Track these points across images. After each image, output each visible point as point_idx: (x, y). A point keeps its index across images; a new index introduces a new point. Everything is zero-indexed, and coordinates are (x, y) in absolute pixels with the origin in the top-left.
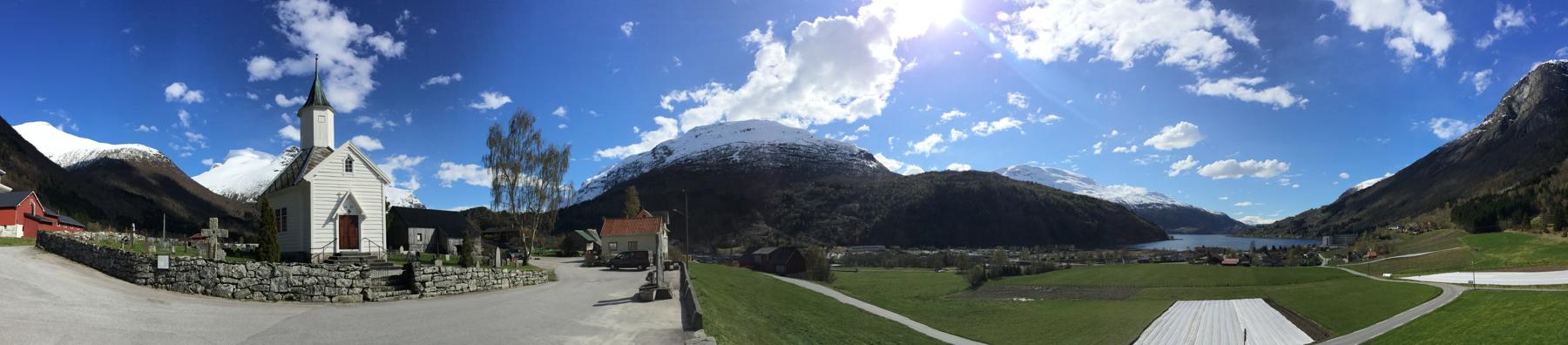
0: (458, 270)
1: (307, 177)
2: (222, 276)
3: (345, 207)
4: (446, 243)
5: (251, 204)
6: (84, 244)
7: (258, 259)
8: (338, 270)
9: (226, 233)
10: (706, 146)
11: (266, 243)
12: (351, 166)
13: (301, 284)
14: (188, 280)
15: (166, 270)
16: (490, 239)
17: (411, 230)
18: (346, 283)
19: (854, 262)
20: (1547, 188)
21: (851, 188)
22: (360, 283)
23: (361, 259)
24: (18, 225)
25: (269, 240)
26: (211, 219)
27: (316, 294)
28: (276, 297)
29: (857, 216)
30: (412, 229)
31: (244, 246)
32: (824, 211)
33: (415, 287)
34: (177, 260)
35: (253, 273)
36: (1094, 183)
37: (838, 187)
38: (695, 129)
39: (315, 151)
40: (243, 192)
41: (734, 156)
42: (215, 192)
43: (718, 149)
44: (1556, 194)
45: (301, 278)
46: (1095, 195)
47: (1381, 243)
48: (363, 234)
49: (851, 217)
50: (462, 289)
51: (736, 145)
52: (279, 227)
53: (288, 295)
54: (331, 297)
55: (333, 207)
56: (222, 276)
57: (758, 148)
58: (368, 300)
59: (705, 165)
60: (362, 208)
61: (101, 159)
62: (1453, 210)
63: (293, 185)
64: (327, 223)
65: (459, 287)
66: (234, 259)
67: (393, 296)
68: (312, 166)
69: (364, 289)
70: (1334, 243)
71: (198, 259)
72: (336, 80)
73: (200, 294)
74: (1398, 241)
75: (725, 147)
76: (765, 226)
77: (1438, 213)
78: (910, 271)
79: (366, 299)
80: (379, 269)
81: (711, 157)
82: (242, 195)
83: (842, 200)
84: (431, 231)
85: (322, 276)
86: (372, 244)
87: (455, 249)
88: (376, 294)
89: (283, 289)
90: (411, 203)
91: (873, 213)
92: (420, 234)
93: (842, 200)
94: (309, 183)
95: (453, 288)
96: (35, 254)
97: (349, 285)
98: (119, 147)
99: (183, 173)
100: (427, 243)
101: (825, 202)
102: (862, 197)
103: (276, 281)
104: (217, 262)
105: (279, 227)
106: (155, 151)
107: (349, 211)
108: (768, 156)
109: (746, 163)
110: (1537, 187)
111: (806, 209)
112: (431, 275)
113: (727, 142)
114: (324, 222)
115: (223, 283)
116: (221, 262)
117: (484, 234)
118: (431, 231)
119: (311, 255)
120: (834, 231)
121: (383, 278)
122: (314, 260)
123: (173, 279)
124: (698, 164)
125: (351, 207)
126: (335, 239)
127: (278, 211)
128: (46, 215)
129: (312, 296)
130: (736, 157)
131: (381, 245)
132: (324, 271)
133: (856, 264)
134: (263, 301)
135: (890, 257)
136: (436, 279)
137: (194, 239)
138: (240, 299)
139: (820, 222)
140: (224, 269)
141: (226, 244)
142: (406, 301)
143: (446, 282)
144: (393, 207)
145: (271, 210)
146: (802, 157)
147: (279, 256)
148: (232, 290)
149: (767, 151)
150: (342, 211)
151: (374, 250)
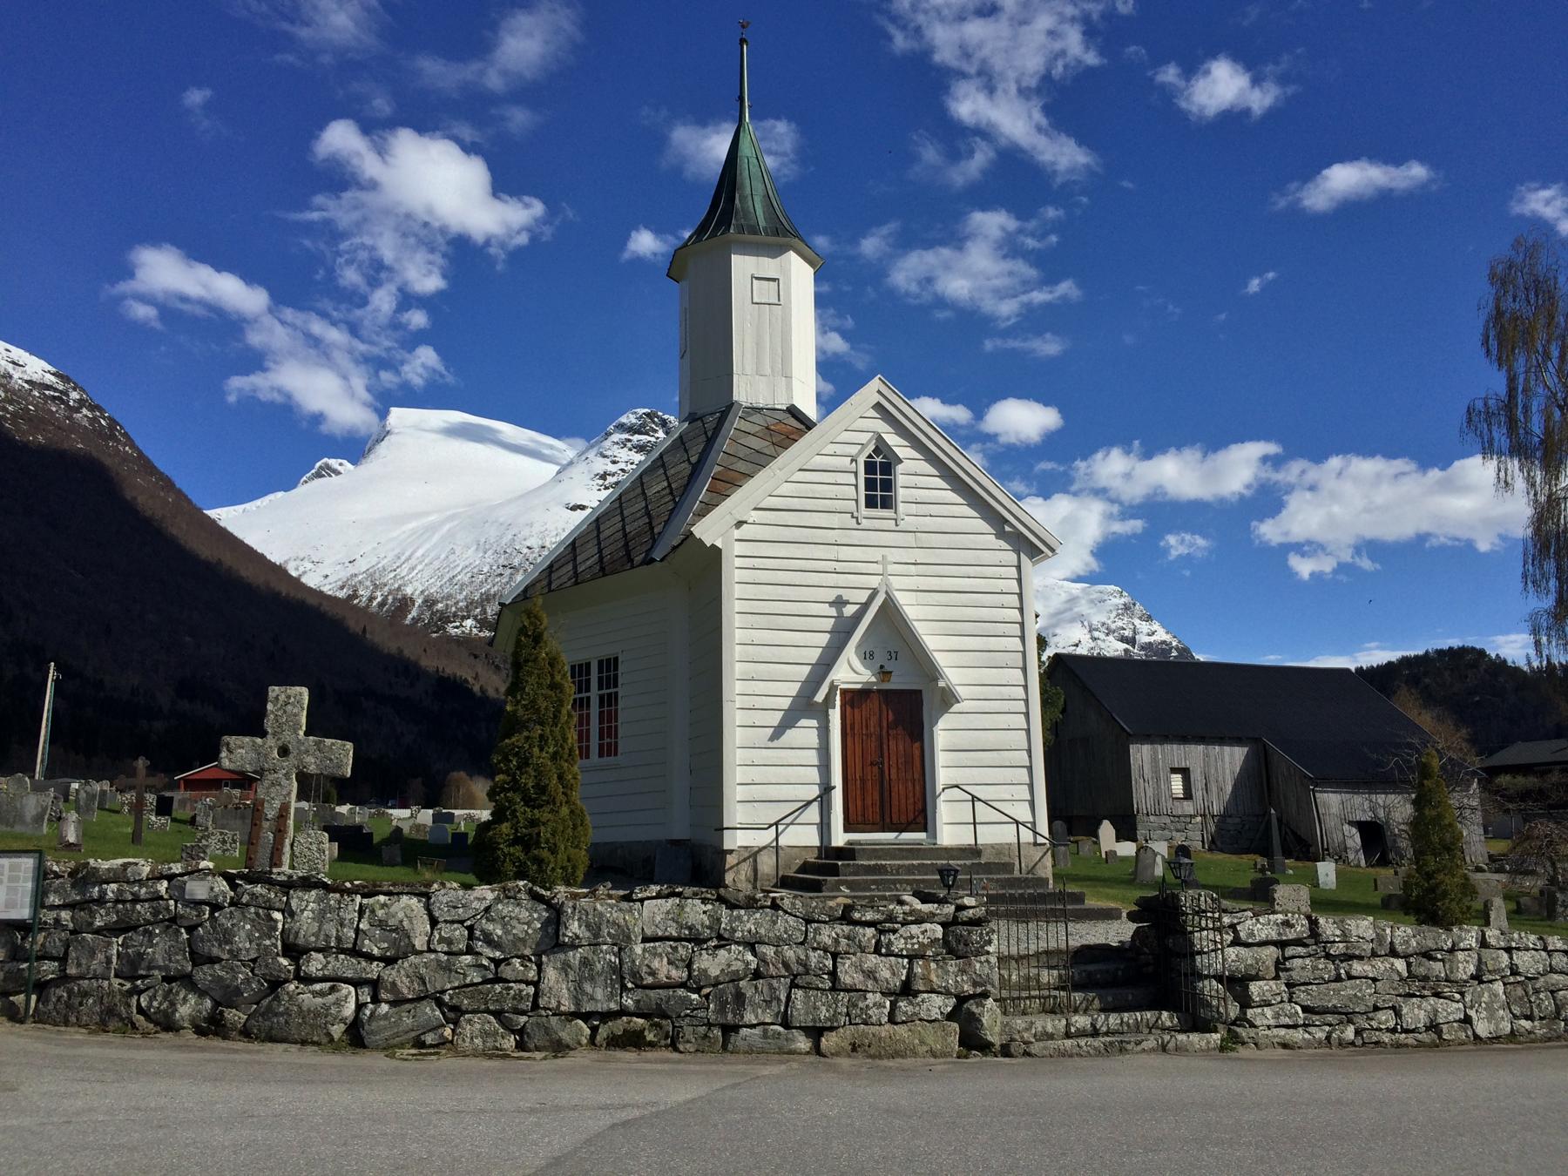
0: (1404, 933)
1: (709, 530)
3: (867, 656)
4: (1307, 808)
5: (465, 641)
7: (489, 874)
8: (846, 917)
9: (342, 756)
11: (527, 801)
12: (888, 485)
13: (678, 974)
14: (132, 968)
16: (1525, 795)
17: (1141, 755)
18: (885, 974)
22: (951, 975)
23: (944, 872)
25: (542, 789)
26: (274, 691)
27: (750, 1017)
28: (565, 1035)
30: (1146, 748)
31: (426, 816)
33: (1200, 1001)
34: (83, 878)
35: (460, 933)
39: (736, 423)
45: (683, 950)
48: (945, 771)
50: (1433, 1027)
52: (583, 736)
53: (618, 1026)
54: (815, 1033)
55: (814, 655)
56: (306, 951)
58: (985, 1047)
60: (941, 660)
63: (649, 561)
64: (789, 721)
65: (1416, 1013)
66: (371, 872)
67: (1095, 1033)
68: (727, 484)
69: (962, 999)
71: (194, 872)
72: (946, 12)
73: (189, 1035)
79: (973, 1041)
80: (1022, 917)
82: (429, 602)
84: (1232, 758)
85: (778, 943)
86: (983, 812)
87: (1354, 839)
88: (1019, 1023)
89: (600, 997)
90: (1131, 641)
92: (1185, 772)
94: (716, 553)
95: (1386, 1018)
97: (896, 983)
99: (169, 484)
100: (1217, 808)
104: (288, 886)
105: (583, 736)
107: (884, 673)
112: (1271, 952)
114: (775, 718)
115: (308, 980)
116: (307, 884)
117: (1494, 771)
118: (1232, 758)
119: (723, 853)
121: (1048, 957)
122: (737, 878)
125: (893, 655)
126: (827, 789)
127: (581, 670)
129: (729, 1030)
131: (1023, 813)
132: (787, 924)
134: (501, 1055)
136: (1301, 966)
137: (191, 784)
138: (389, 1048)
140: (320, 917)
141: (344, 809)
142: (1158, 1060)
143: (1348, 989)
144: (1057, 656)
145: (553, 661)
147: (582, 858)
148: (349, 1009)
150: (851, 672)
151: (995, 835)
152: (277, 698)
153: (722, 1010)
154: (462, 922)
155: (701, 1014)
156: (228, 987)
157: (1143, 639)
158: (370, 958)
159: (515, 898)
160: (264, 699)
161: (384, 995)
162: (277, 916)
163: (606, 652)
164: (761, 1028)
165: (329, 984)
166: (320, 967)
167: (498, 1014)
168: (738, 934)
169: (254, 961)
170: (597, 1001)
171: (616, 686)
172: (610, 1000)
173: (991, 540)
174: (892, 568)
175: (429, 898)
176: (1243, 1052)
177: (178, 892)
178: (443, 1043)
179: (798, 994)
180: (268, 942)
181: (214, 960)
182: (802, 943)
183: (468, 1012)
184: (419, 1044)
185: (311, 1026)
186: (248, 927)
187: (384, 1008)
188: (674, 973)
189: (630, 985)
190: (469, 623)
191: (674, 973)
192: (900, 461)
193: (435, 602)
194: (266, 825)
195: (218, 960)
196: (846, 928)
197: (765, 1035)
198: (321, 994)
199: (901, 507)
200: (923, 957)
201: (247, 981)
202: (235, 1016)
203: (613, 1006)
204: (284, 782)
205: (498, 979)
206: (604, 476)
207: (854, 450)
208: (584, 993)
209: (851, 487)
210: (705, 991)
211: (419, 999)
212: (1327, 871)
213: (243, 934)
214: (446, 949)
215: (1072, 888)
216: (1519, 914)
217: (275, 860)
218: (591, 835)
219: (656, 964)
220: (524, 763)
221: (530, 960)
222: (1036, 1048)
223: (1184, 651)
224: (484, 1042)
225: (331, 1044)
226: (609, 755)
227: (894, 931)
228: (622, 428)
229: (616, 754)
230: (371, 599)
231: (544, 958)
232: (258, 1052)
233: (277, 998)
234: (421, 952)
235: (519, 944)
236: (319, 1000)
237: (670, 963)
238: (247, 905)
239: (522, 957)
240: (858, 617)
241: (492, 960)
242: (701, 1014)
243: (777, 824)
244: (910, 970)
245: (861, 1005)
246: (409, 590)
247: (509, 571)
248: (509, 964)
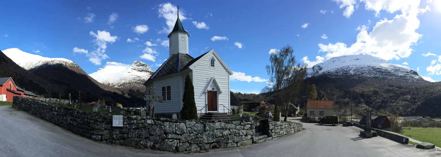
2: (168, 133)
3: (211, 86)
5: (116, 88)
6: (46, 105)
10: (337, 66)
12: (213, 64)
13: (221, 135)
15: (120, 128)
19: (408, 125)
21: (406, 88)
24: (4, 95)
27: (230, 142)
29: (409, 102)
32: (393, 99)
37: (400, 88)
38: (333, 58)
40: (113, 82)
41: (351, 71)
42: (99, 82)
43: (343, 68)
49: (406, 102)
51: (352, 66)
53: (213, 145)
54: (237, 143)
55: (204, 86)
56: (168, 133)
57: (362, 68)
59: (337, 75)
60: (220, 87)
61: (44, 64)
71: (147, 118)
75: (347, 67)
76: (365, 105)
78: (436, 129)
81: (340, 72)
82: (112, 84)
83: (403, 94)
91: (417, 100)
93: (403, 94)
94: (192, 70)
96: (12, 111)
98: (53, 59)
101: (394, 94)
102: (412, 92)
103: (206, 134)
106: (71, 62)
107: (213, 89)
108: (367, 72)
109: (356, 75)
111: (384, 98)
113: (348, 65)
114: (199, 94)
115: (169, 139)
120: (398, 109)
123: (125, 135)
124: (334, 75)
128: (18, 90)
130: (352, 72)
133: (409, 125)
135: (425, 122)
138: (182, 152)
139: (391, 104)
146: (383, 73)
149: (366, 69)
150: (209, 89)
152: (152, 89)
153: (226, 141)
154: (191, 127)
155: (224, 141)
156: (156, 140)
158: (178, 134)
159: (198, 123)
161: (181, 141)
162: (163, 127)
164: (231, 143)
165: (172, 140)
166: (170, 136)
167: (197, 144)
168: (228, 128)
169: (160, 135)
170: (211, 141)
171: (170, 90)
172: (212, 140)
173: (225, 72)
174: (215, 75)
175: (185, 123)
179: (235, 137)
180: (162, 132)
182: (235, 129)
183: (193, 144)
185: (170, 148)
186: (158, 129)
187: (181, 144)
188: (220, 135)
189: (215, 137)
190: (117, 86)
191: (220, 135)
192: (215, 61)
193: (113, 84)
194: (151, 110)
195: (153, 135)
196: (240, 126)
197: (231, 144)
198: (171, 142)
199: (215, 67)
200: (248, 130)
201: (159, 139)
202: (157, 146)
203: (213, 141)
204: (153, 103)
205: (197, 138)
206: (132, 69)
207: (210, 58)
208: (209, 139)
209: (209, 63)
210: (224, 137)
211: (186, 142)
213: (157, 130)
214: (189, 132)
219: (218, 133)
221: (201, 134)
224: (195, 149)
226: (169, 100)
227: (245, 126)
228: (134, 63)
229: (170, 100)
230: (106, 84)
231: (203, 134)
232: (164, 153)
233: (164, 142)
234: (186, 133)
235: (199, 131)
236: (171, 143)
237: (220, 133)
238: (158, 125)
239: (200, 133)
241: (195, 134)
242: (224, 141)
243: (201, 110)
244: (247, 132)
245: (242, 138)
246: (110, 82)
247: (121, 80)
248: (198, 135)
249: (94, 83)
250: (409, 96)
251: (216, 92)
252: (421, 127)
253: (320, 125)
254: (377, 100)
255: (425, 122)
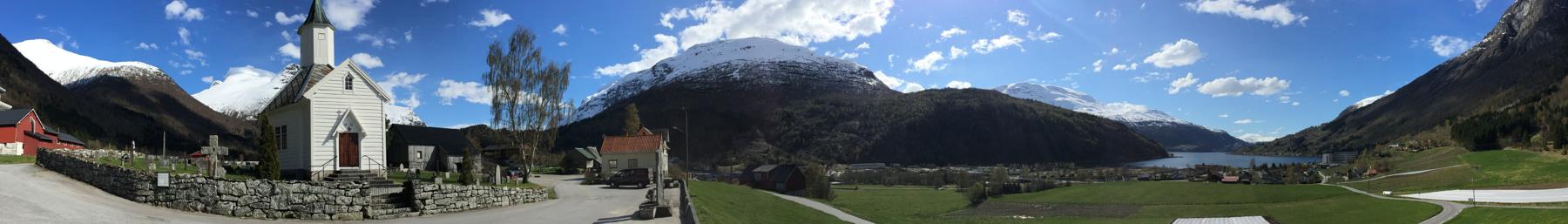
0: (458, 188)
1: (307, 95)
2: (222, 194)
3: (345, 125)
4: (446, 160)
6: (84, 162)
7: (258, 177)
8: (338, 188)
9: (226, 150)
12: (351, 84)
13: (301, 201)
14: (188, 197)
15: (166, 188)
16: (490, 157)
17: (411, 148)
20: (1547, 106)
21: (851, 106)
22: (360, 200)
23: (361, 176)
25: (269, 158)
26: (211, 137)
28: (276, 215)
31: (244, 163)
33: (415, 205)
34: (177, 178)
36: (1093, 101)
38: (695, 47)
40: (243, 109)
41: (734, 73)
42: (215, 109)
44: (1556, 112)
45: (301, 195)
46: (1095, 113)
47: (1382, 161)
48: (363, 152)
49: (851, 135)
50: (462, 207)
51: (736, 63)
52: (279, 144)
53: (288, 213)
54: (331, 215)
55: (333, 125)
56: (222, 194)
58: (368, 217)
59: (705, 83)
60: (362, 126)
61: (101, 77)
62: (1453, 127)
63: (293, 102)
64: (326, 141)
65: (459, 204)
67: (393, 213)
68: (312, 83)
69: (363, 206)
70: (1334, 160)
73: (200, 212)
74: (1398, 158)
76: (765, 143)
77: (1438, 130)
78: (910, 188)
79: (366, 216)
80: (378, 187)
82: (242, 113)
84: (431, 149)
85: (322, 194)
87: (455, 167)
88: (376, 211)
90: (411, 121)
91: (873, 130)
92: (421, 152)
94: (309, 100)
95: (453, 206)
97: (349, 203)
100: (427, 160)
101: (826, 119)
104: (217, 180)
105: (279, 144)
106: (155, 69)
107: (349, 129)
109: (746, 81)
110: (1537, 105)
111: (806, 127)
113: (727, 61)
114: (324, 140)
115: (223, 201)
116: (221, 179)
117: (485, 151)
118: (431, 149)
120: (835, 148)
122: (314, 178)
125: (351, 125)
126: (335, 157)
127: (278, 129)
128: (46, 132)
129: (312, 214)
130: (736, 75)
132: (324, 189)
133: (856, 181)
134: (262, 218)
135: (889, 175)
136: (436, 196)
137: (194, 156)
138: (240, 216)
142: (406, 219)
143: (446, 200)
144: (393, 124)
147: (279, 173)
149: (767, 69)
150: (342, 129)
151: (374, 167)
157: (414, 120)
160: (209, 138)
163: (284, 124)
173: (375, 97)
176: (424, 216)
177: (196, 181)
178: (250, 216)
181: (204, 196)
184: (246, 216)
202: (209, 209)
212: (448, 175)
215: (390, 180)
216: (481, 183)
217: (214, 174)
218: (281, 168)
220: (265, 151)
222: (379, 217)
223: (424, 124)
225: (229, 215)
228: (287, 68)
240: (343, 116)
249: (200, 114)
250: (858, 123)
251: (357, 134)
252: (880, 184)
253: (611, 187)
254: (792, 132)
255: (889, 175)
